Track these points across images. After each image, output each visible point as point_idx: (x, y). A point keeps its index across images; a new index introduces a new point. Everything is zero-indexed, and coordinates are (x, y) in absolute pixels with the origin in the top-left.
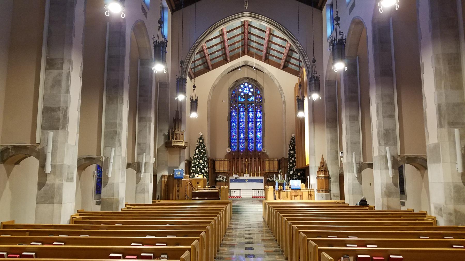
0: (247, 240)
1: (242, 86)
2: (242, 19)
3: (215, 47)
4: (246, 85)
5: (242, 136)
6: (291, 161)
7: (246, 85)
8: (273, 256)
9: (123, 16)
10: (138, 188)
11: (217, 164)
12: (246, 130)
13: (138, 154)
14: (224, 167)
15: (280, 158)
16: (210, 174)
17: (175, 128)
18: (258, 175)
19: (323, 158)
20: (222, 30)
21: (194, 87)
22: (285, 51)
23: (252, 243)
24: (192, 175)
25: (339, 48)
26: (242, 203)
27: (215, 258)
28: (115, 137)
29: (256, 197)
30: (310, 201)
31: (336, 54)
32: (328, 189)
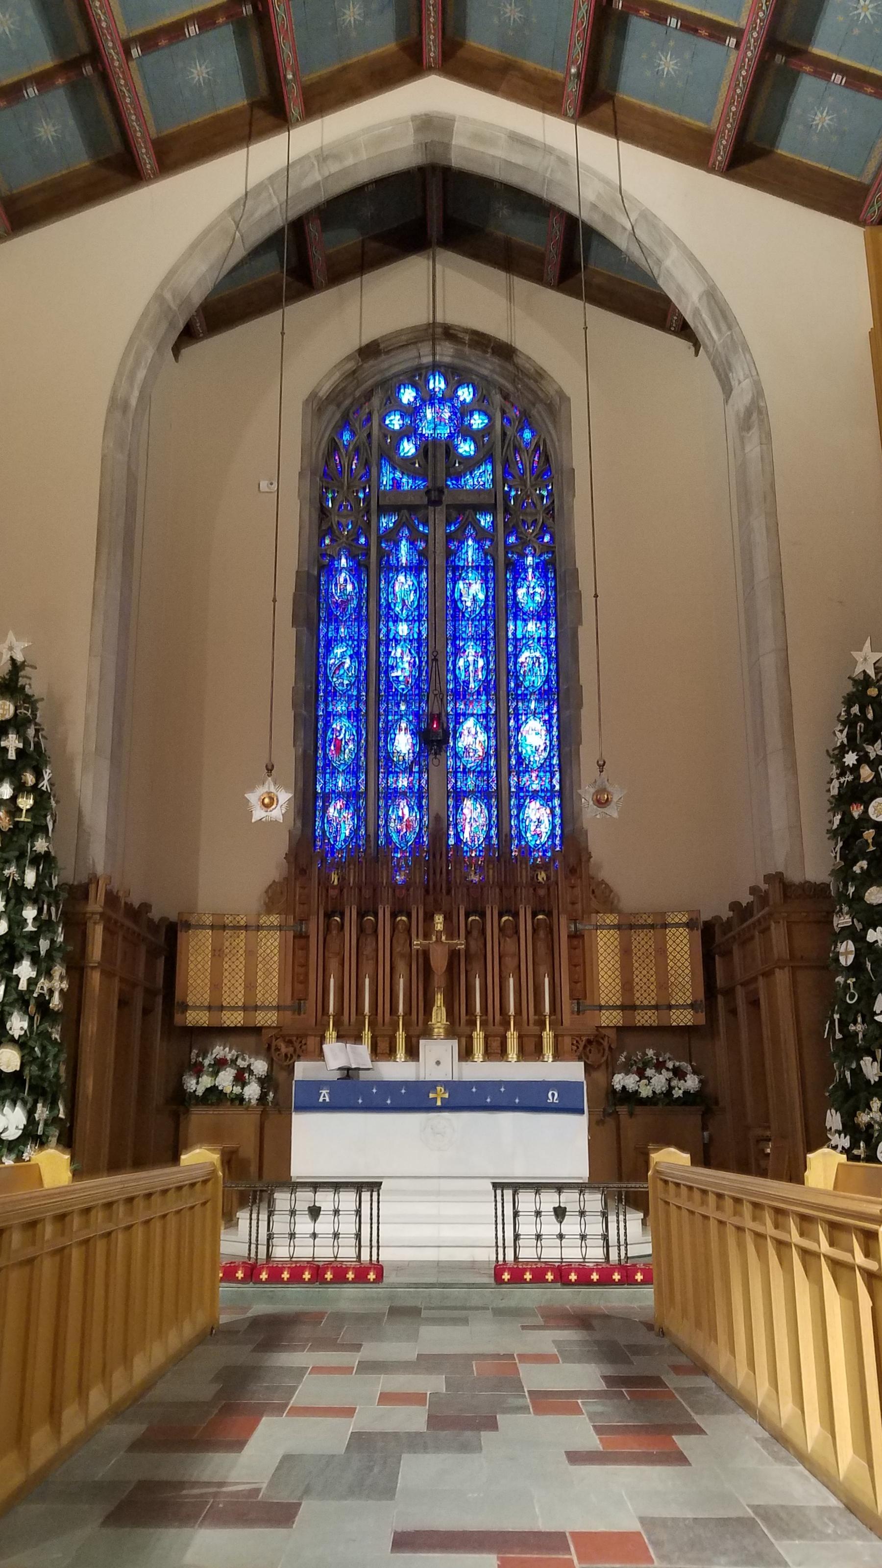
11: (197, 956)
16: (91, 1027)
18: (531, 1050)
29: (539, 1276)
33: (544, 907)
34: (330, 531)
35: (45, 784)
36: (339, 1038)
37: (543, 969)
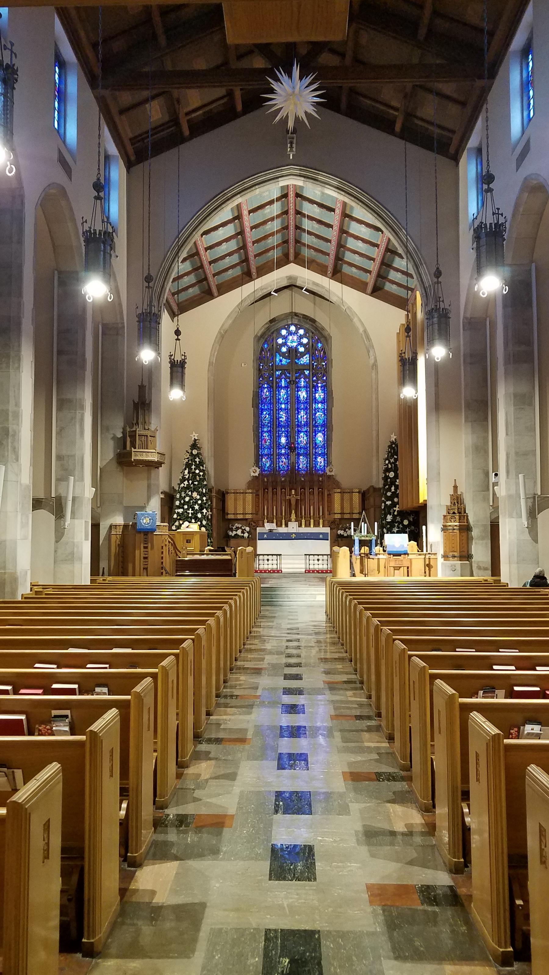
0: (284, 660)
1: (284, 332)
2: (283, 182)
3: (224, 246)
4: (293, 328)
5: (283, 440)
6: (389, 494)
7: (293, 328)
8: (341, 692)
9: (10, 172)
10: (59, 552)
11: (230, 500)
12: (292, 428)
13: (58, 480)
14: (244, 509)
15: (364, 488)
16: (214, 522)
17: (137, 423)
18: (317, 525)
19: (455, 487)
20: (239, 207)
21: (178, 332)
22: (377, 254)
23: (299, 665)
24: (177, 523)
25: (490, 240)
26: (284, 583)
27: (218, 696)
28: (4, 443)
29: (313, 571)
30: (428, 579)
31: (483, 255)
32: (465, 554)
33: (321, 487)
34: (261, 376)
35: (204, 469)
36: (268, 522)
37: (321, 503)
